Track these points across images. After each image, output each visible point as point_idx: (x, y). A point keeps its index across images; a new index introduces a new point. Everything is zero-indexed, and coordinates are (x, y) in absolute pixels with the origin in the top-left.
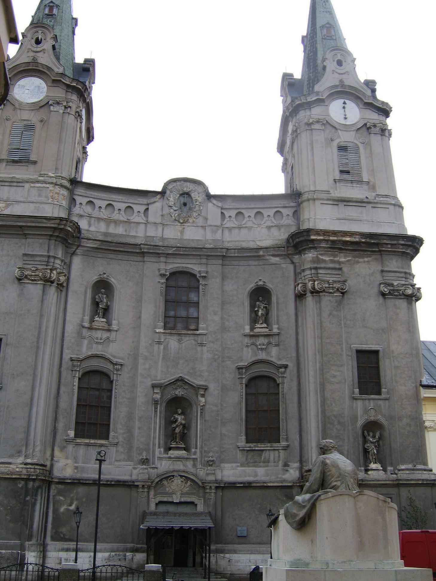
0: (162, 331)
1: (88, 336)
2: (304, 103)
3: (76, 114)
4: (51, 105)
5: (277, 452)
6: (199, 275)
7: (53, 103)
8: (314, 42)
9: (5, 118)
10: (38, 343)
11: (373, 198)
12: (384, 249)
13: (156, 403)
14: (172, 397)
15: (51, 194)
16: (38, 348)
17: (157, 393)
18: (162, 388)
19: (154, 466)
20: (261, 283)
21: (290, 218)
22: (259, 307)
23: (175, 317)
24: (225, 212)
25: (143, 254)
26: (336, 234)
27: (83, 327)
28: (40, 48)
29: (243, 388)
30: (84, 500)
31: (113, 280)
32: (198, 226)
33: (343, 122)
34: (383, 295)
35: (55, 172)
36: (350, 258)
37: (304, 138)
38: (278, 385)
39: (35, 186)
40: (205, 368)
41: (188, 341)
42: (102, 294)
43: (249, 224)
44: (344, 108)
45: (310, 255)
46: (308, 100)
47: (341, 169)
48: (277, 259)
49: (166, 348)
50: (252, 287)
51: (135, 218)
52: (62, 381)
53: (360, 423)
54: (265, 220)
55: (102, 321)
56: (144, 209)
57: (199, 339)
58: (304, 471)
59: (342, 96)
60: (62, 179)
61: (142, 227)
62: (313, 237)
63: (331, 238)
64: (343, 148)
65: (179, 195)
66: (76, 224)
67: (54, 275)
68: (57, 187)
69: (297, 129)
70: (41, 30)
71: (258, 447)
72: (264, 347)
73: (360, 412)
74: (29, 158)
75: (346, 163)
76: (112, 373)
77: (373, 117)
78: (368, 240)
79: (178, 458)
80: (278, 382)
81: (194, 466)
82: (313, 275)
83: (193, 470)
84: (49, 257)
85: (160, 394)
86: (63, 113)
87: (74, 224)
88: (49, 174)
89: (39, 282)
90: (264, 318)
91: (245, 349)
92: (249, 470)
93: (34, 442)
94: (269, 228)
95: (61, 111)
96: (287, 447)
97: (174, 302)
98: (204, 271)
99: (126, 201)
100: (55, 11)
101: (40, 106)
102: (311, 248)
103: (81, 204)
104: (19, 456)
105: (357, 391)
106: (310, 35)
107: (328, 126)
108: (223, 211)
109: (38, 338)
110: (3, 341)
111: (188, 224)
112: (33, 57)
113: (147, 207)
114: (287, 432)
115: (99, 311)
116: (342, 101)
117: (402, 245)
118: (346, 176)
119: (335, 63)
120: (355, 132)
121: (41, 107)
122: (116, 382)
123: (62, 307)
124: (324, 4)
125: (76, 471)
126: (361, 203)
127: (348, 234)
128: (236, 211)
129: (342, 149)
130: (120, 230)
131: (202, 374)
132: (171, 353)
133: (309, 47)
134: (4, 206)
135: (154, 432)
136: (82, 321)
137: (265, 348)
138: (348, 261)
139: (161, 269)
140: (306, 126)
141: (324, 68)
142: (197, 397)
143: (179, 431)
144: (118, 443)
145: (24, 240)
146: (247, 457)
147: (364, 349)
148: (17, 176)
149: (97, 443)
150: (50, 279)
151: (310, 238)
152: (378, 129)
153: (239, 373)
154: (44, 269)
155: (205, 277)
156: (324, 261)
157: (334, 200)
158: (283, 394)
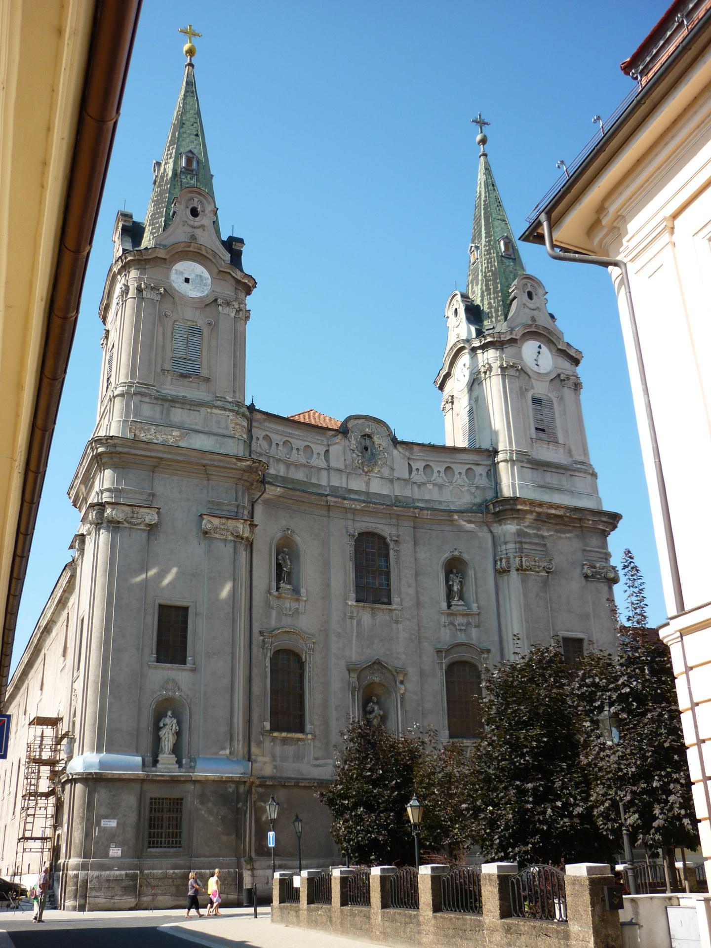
12: (585, 525)
20: (456, 553)
24: (412, 463)
28: (198, 221)
30: (285, 806)
31: (298, 538)
33: (536, 368)
34: (586, 577)
36: (552, 533)
41: (382, 617)
45: (510, 528)
46: (502, 339)
48: (473, 526)
49: (359, 624)
50: (447, 557)
52: (254, 661)
62: (519, 507)
91: (442, 629)
95: (233, 315)
103: (277, 444)
113: (327, 449)
116: (539, 344)
118: (541, 435)
119: (526, 294)
121: (206, 305)
125: (275, 771)
128: (424, 464)
129: (537, 401)
138: (551, 536)
155: (396, 541)
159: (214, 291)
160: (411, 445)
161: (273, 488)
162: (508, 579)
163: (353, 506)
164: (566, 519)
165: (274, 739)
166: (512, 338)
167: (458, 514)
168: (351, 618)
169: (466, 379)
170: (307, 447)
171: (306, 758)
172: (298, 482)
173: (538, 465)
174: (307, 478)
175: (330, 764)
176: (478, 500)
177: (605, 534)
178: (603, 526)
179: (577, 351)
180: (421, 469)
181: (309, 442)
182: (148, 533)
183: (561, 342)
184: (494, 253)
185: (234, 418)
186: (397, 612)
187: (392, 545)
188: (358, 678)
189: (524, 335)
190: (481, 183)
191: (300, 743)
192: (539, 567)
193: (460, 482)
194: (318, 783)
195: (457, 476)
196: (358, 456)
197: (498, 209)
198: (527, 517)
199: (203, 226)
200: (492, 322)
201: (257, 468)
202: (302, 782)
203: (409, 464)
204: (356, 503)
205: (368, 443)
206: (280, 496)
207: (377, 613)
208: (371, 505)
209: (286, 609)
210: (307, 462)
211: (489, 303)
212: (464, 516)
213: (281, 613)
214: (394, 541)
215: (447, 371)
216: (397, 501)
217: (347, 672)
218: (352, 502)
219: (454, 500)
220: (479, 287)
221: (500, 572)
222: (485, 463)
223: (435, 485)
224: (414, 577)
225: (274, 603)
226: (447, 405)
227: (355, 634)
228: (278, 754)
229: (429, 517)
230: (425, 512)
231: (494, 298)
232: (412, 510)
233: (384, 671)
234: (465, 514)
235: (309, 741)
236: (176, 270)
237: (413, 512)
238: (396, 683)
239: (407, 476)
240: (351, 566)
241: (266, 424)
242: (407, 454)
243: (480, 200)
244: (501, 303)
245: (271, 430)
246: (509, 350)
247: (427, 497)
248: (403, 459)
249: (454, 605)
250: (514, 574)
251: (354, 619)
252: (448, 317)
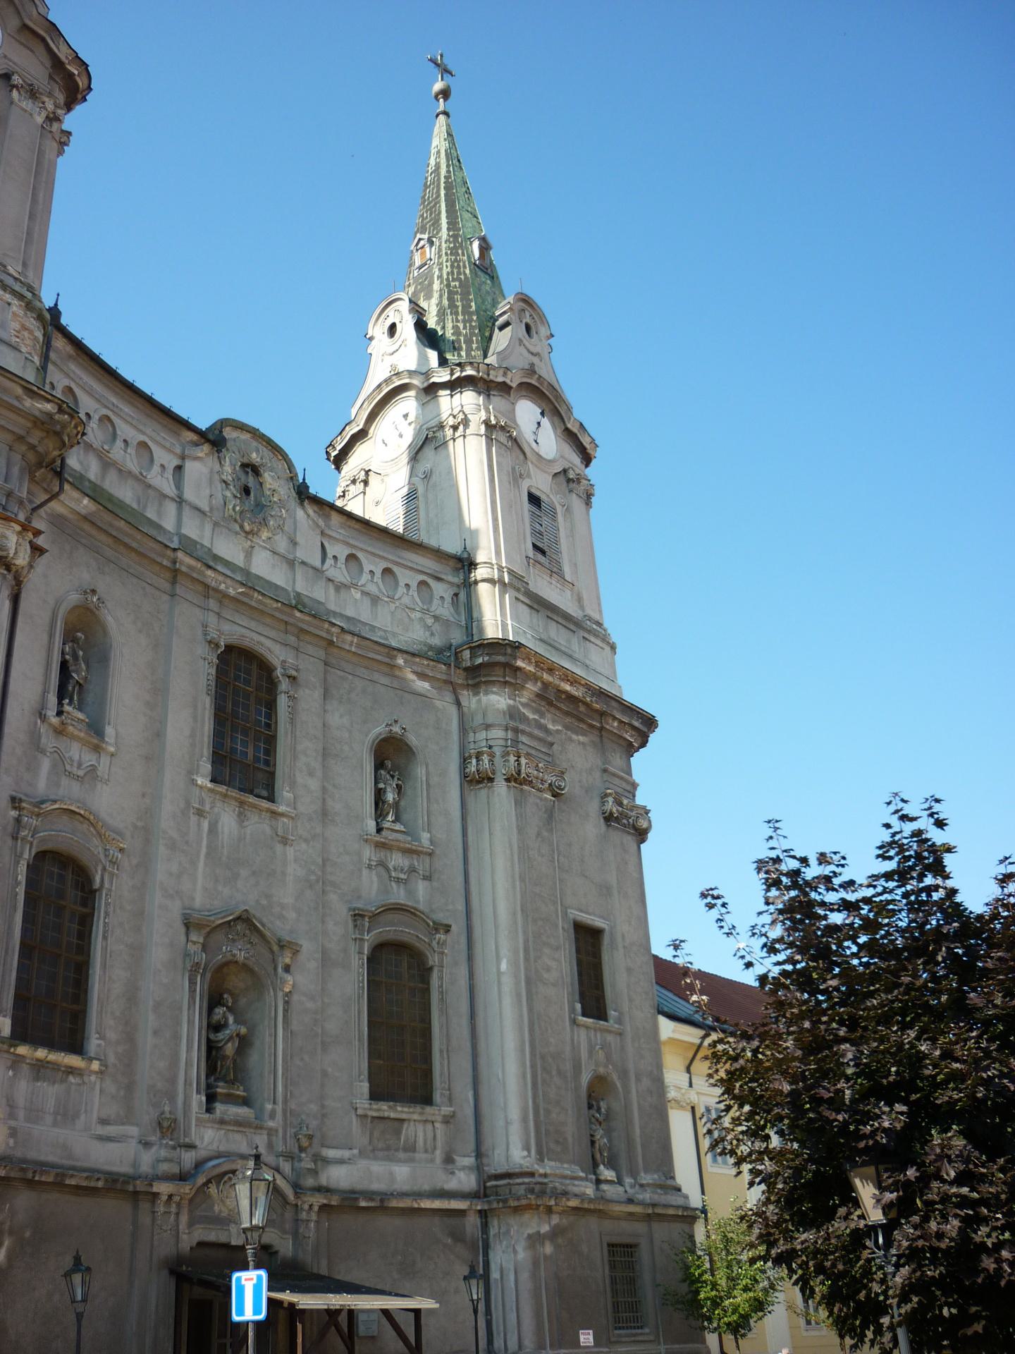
7: (22, 86)
12: (608, 727)
20: (396, 729)
24: (326, 544)
29: (363, 965)
30: (27, 1234)
31: (109, 618)
36: (560, 728)
40: (289, 900)
41: (258, 825)
45: (497, 700)
48: (426, 685)
49: (213, 830)
50: (380, 734)
62: (520, 663)
71: (397, 1111)
72: (402, 876)
79: (240, 1124)
91: (365, 872)
92: (377, 1167)
117: (634, 728)
118: (540, 557)
125: (11, 1142)
128: (347, 551)
129: (534, 500)
131: (284, 913)
132: (223, 847)
146: (371, 1134)
155: (294, 678)
159: (5, 57)
160: (328, 509)
161: (76, 494)
162: (488, 797)
163: (223, 587)
164: (582, 708)
165: (17, 1061)
166: (504, 382)
167: (405, 656)
168: (200, 813)
169: (409, 435)
170: (143, 445)
171: (83, 1117)
172: (121, 504)
173: (538, 604)
174: (139, 503)
175: (132, 1137)
176: (436, 641)
177: (630, 750)
178: (632, 736)
180: (342, 558)
183: (572, 419)
184: (463, 255)
185: (21, 313)
186: (285, 820)
187: (284, 685)
188: (204, 947)
189: (521, 384)
190: (438, 152)
191: (71, 1079)
192: (543, 781)
193: (406, 600)
194: (106, 1181)
195: (402, 590)
196: (235, 497)
197: (466, 196)
198: (527, 686)
200: (459, 355)
201: (64, 426)
202: (72, 1176)
203: (322, 544)
204: (229, 581)
205: (251, 481)
206: (85, 518)
207: (248, 814)
208: (256, 595)
209: (72, 761)
210: (141, 474)
211: (455, 328)
212: (415, 663)
213: (61, 766)
214: (289, 677)
215: (360, 427)
216: (299, 604)
217: (183, 930)
218: (221, 578)
219: (396, 630)
220: (434, 301)
221: (470, 782)
222: (450, 578)
223: (364, 593)
224: (320, 759)
225: (48, 741)
226: (352, 488)
227: (204, 850)
228: (21, 1101)
229: (353, 649)
230: (349, 638)
231: (464, 321)
232: (326, 626)
233: (255, 939)
234: (418, 660)
235: (93, 1078)
237: (328, 632)
238: (275, 969)
239: (318, 563)
240: (206, 705)
241: (73, 366)
242: (321, 522)
243: (439, 175)
244: (477, 331)
245: (81, 383)
246: (498, 401)
247: (350, 612)
248: (313, 530)
249: (388, 829)
250: (501, 787)
252: (371, 339)
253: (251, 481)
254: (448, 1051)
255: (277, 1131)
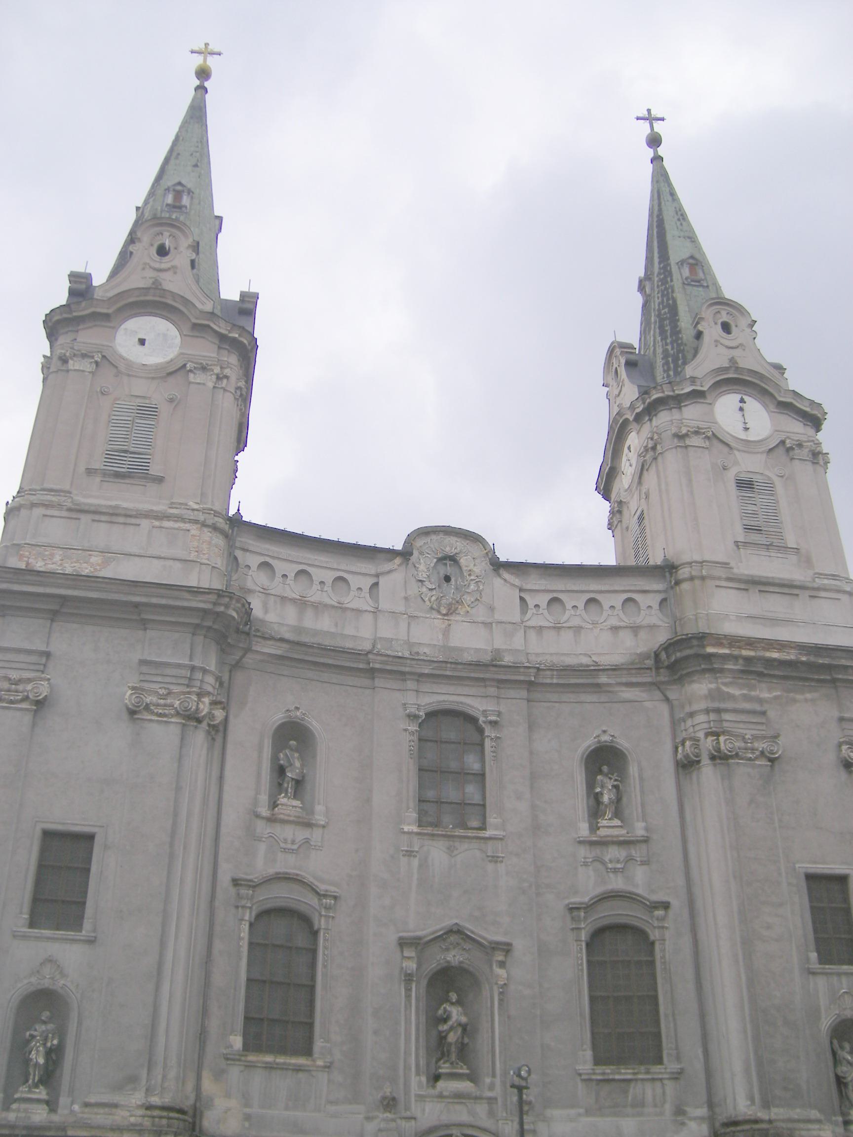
0: (415, 829)
1: (267, 836)
2: (668, 397)
3: (236, 392)
4: (190, 371)
5: (658, 1084)
6: (484, 719)
8: (668, 289)
9: (98, 390)
10: (171, 845)
11: (809, 579)
13: (409, 980)
14: (439, 967)
15: (195, 544)
16: (172, 856)
17: (409, 958)
18: (419, 948)
19: (408, 1114)
20: (605, 738)
21: (653, 612)
22: (602, 787)
23: (439, 802)
25: (372, 673)
26: (754, 645)
27: (258, 816)
28: (166, 262)
29: (581, 949)
31: (314, 723)
32: (474, 622)
33: (742, 435)
35: (201, 501)
36: (779, 693)
37: (671, 461)
38: (653, 944)
39: (163, 525)
41: (468, 852)
42: (292, 750)
43: (576, 622)
44: (741, 409)
45: (701, 687)
46: (677, 392)
47: (746, 522)
50: (589, 746)
51: (353, 601)
53: (826, 1023)
54: (605, 614)
55: (293, 807)
56: (371, 584)
57: (490, 848)
58: (717, 1125)
59: (735, 387)
60: (214, 516)
61: (369, 618)
62: (710, 650)
63: (745, 653)
64: (742, 483)
65: (435, 560)
66: (247, 606)
67: (205, 707)
68: (206, 530)
69: (656, 445)
70: (168, 231)
71: (620, 1073)
72: (619, 866)
73: (823, 1002)
74: (148, 470)
75: (753, 512)
76: (317, 914)
77: (796, 428)
78: (812, 659)
79: (459, 1096)
80: (652, 938)
81: (491, 1113)
82: (712, 723)
83: (487, 1123)
84: (193, 669)
85: (416, 960)
86: (214, 387)
87: (243, 605)
88: (189, 504)
89: (173, 720)
90: (614, 807)
93: (165, 1059)
94: (615, 629)
95: (210, 385)
96: (679, 1073)
97: (436, 771)
98: (495, 711)
99: (335, 566)
100: (185, 200)
101: (168, 372)
102: (704, 671)
104: (134, 1089)
105: (814, 956)
106: (657, 276)
107: (715, 442)
108: (523, 595)
109: (173, 834)
110: (97, 839)
111: (458, 618)
112: (153, 280)
114: (676, 1041)
115: (286, 785)
116: (738, 397)
118: (754, 537)
119: (719, 327)
120: (765, 454)
122: (324, 934)
123: (215, 773)
124: (678, 223)
125: (247, 1124)
126: (788, 588)
127: (775, 646)
129: (745, 485)
130: (325, 623)
133: (658, 298)
134: (100, 562)
135: (406, 1040)
136: (255, 802)
137: (622, 868)
138: (776, 698)
139: (407, 704)
140: (676, 440)
141: (699, 335)
142: (491, 967)
143: (454, 1040)
144: (331, 1063)
145: (141, 632)
147: (819, 871)
148: (125, 505)
149: (290, 1064)
150: (196, 713)
151: (705, 651)
152: (806, 451)
153: (573, 919)
154: (184, 693)
156: (731, 697)
157: (739, 581)
158: (665, 963)
166: (694, 391)
179: (812, 402)
181: (343, 571)
182: (35, 716)
183: (782, 391)
189: (717, 385)
192: (753, 750)
199: (174, 269)
236: (126, 329)
251: (415, 856)
253: (449, 570)
254: (674, 1015)
255: (496, 1099)
